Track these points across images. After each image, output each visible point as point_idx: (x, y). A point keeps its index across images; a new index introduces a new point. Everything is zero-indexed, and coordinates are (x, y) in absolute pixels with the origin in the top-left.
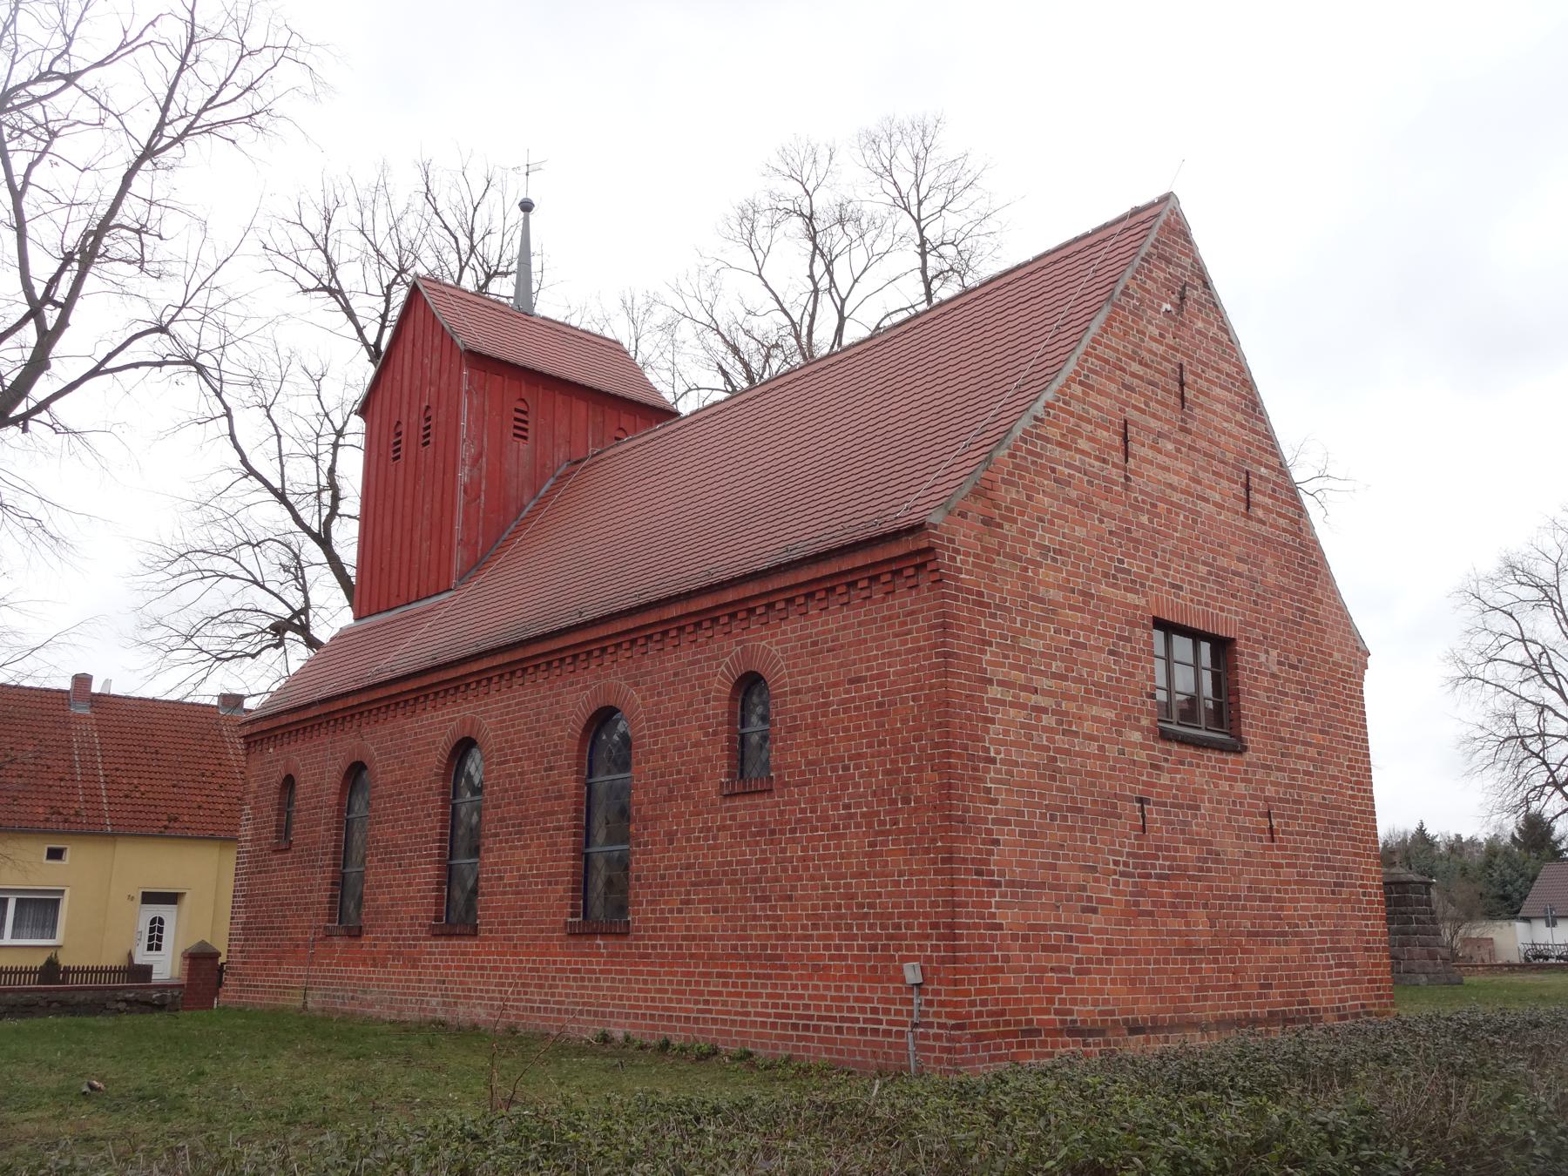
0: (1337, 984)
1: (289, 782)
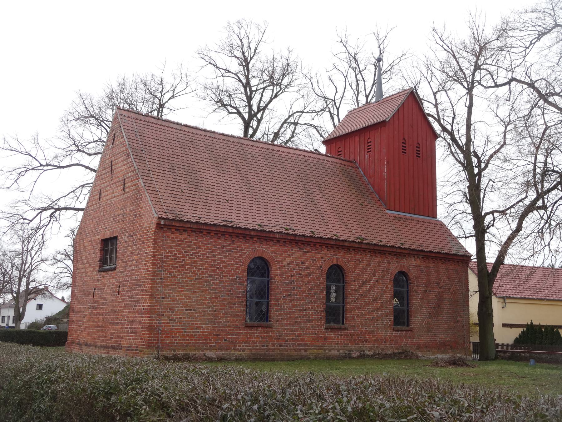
0: (130, 339)
1: (504, 325)
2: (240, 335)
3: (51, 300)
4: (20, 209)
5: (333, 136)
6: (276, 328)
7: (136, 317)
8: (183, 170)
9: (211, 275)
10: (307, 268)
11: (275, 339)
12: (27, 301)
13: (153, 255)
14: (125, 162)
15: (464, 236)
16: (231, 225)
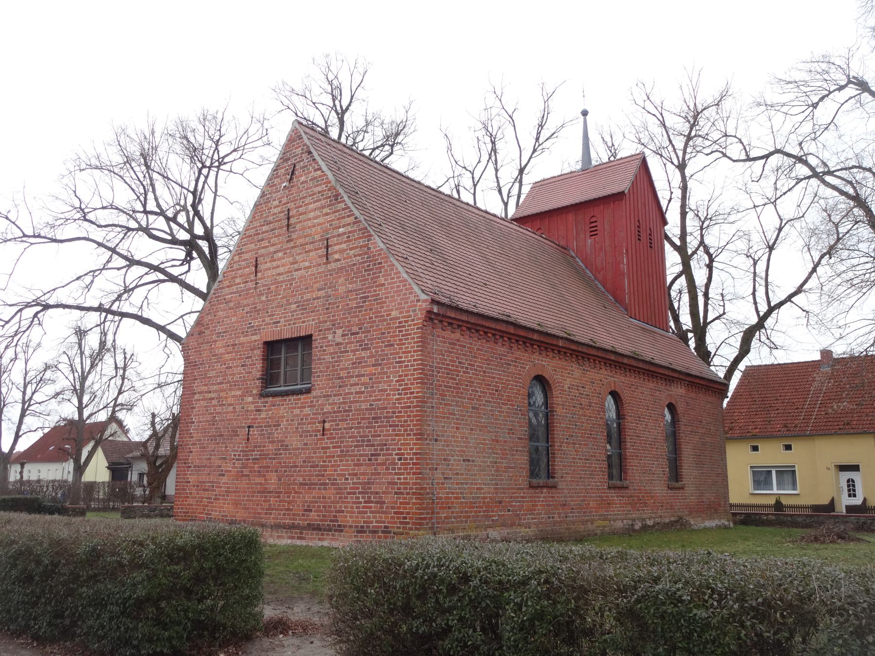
13: (422, 364)
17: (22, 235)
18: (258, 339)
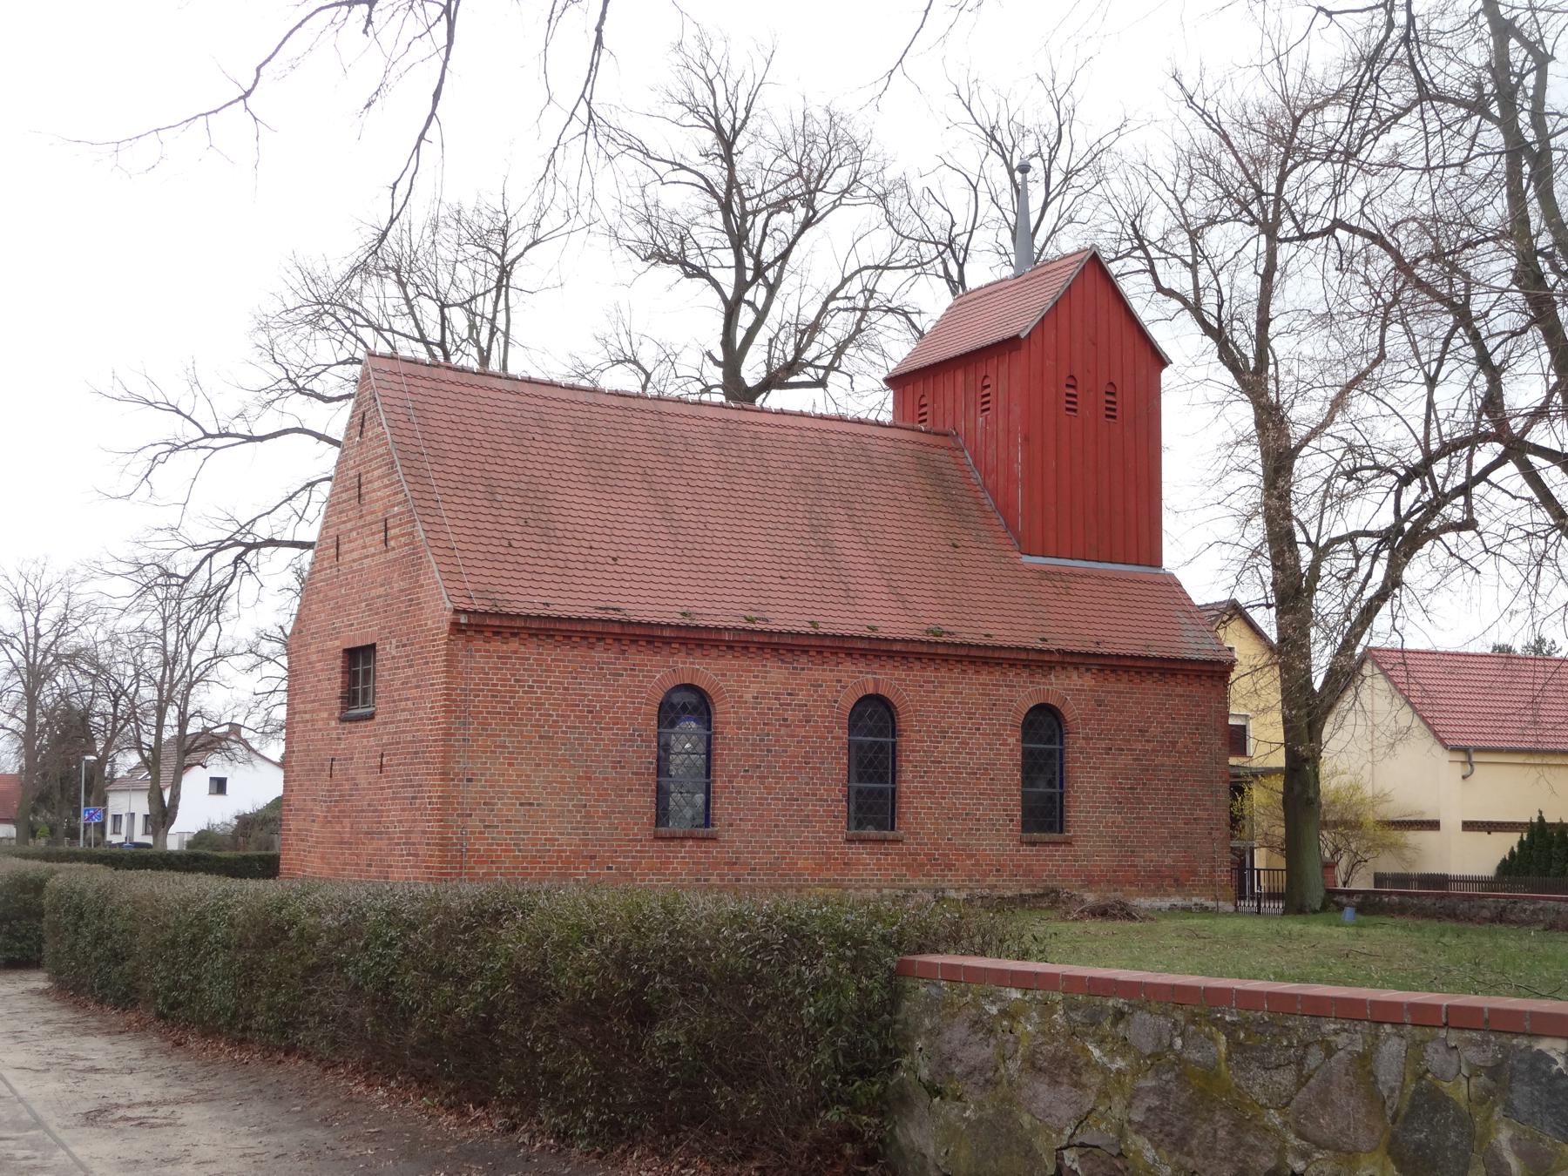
0: (406, 867)
1: (1469, 826)
2: (644, 858)
3: (249, 767)
4: (161, 544)
5: (906, 369)
6: (727, 841)
7: (415, 821)
8: (516, 492)
9: (575, 727)
10: (799, 705)
11: (726, 864)
12: (182, 768)
13: (446, 689)
14: (386, 481)
15: (1263, 601)
16: (618, 617)
17: (202, 435)
18: (338, 645)
